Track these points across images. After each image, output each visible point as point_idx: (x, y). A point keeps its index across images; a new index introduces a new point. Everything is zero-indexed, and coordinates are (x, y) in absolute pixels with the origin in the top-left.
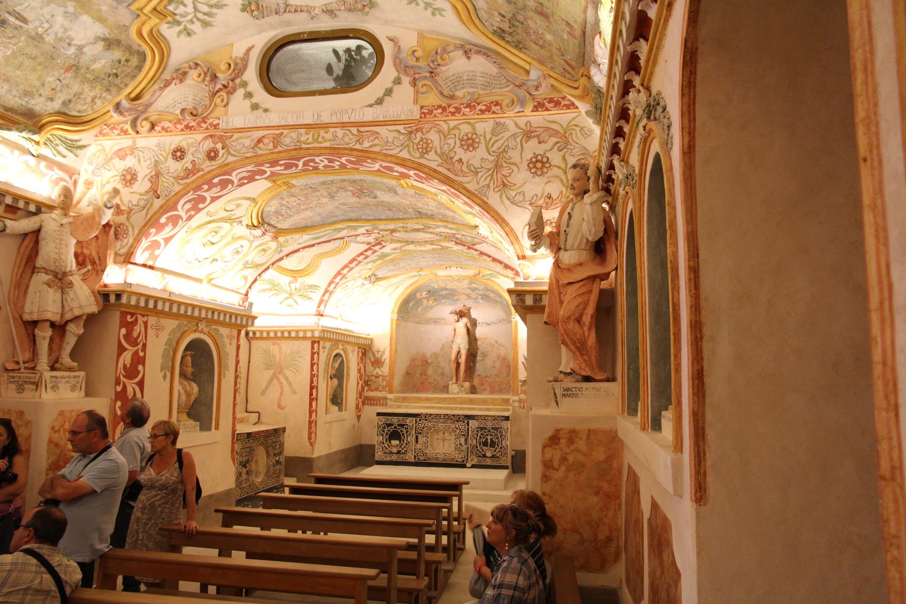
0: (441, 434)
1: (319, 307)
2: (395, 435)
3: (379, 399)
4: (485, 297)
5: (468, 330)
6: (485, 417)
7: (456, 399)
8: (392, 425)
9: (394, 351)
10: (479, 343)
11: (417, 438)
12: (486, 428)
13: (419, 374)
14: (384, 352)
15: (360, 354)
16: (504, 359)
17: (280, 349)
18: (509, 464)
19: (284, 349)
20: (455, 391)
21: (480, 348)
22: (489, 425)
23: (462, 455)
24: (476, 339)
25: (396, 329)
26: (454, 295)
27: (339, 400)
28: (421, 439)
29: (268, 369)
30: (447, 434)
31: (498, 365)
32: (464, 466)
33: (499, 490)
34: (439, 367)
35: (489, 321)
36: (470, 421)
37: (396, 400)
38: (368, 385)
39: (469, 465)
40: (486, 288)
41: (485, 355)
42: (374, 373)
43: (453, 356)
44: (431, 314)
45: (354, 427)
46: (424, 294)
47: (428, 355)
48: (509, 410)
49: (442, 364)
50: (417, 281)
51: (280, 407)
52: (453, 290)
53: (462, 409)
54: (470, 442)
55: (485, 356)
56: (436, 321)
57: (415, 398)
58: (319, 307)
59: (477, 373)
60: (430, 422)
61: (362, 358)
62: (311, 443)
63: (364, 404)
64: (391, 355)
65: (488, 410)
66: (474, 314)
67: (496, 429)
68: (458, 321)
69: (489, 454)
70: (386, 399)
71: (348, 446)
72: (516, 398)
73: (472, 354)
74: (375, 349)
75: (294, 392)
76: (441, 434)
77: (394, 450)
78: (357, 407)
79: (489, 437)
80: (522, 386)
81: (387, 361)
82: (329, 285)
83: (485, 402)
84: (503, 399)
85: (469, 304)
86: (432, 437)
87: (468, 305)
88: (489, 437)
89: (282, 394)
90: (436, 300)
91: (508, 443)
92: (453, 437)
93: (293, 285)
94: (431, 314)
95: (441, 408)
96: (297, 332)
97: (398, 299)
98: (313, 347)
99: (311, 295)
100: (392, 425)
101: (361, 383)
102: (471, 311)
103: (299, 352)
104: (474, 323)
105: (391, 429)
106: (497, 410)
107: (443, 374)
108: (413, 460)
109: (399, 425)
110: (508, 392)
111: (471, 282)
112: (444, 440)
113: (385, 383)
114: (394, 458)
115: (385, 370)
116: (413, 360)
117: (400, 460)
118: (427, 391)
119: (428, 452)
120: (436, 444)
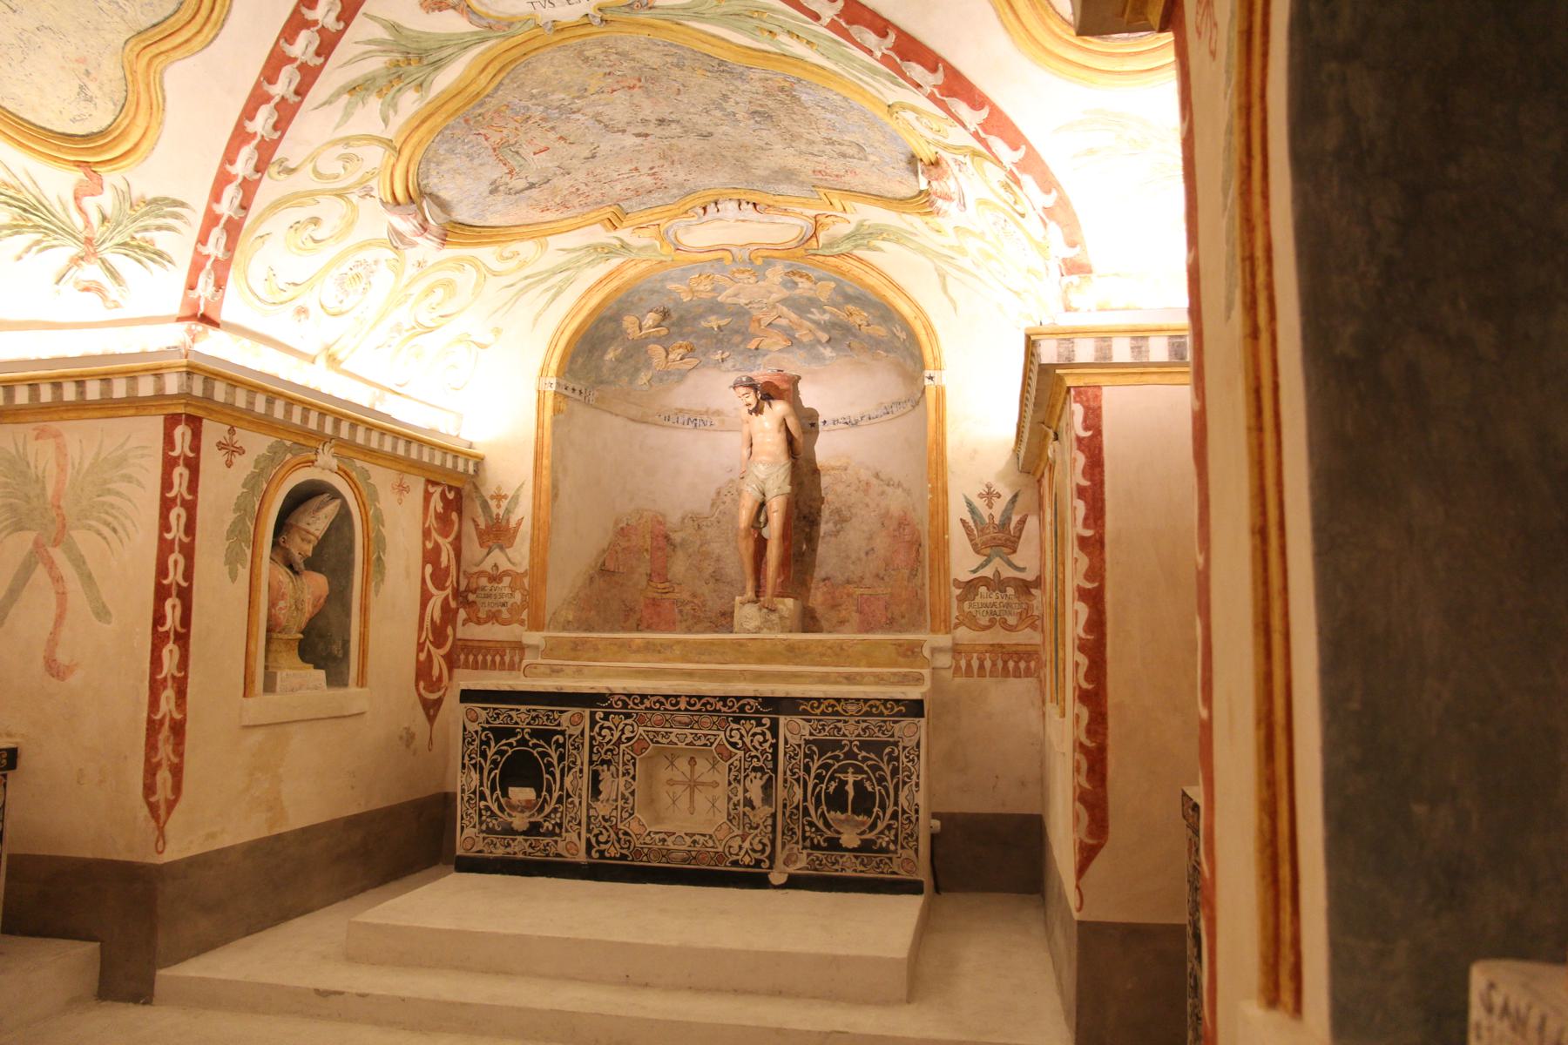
0: (683, 764)
1: (192, 287)
2: (521, 768)
3: (498, 648)
4: (841, 335)
5: (790, 441)
6: (835, 706)
7: (757, 650)
8: (510, 733)
9: (550, 492)
10: (825, 481)
11: (595, 779)
12: (837, 745)
13: (637, 576)
14: (516, 498)
15: (437, 504)
16: (903, 523)
17: (61, 450)
18: (923, 874)
19: (73, 450)
20: (752, 625)
21: (829, 497)
22: (851, 731)
23: (754, 841)
24: (816, 472)
25: (555, 423)
26: (747, 337)
27: (336, 649)
28: (611, 785)
29: (19, 527)
30: (702, 765)
31: (881, 543)
32: (758, 881)
33: (885, 1003)
34: (706, 555)
35: (854, 413)
36: (782, 720)
37: (550, 650)
38: (468, 604)
39: (777, 877)
40: (839, 290)
41: (842, 519)
42: (487, 566)
43: (744, 517)
44: (683, 396)
45: (409, 738)
46: (650, 319)
47: (674, 518)
48: (919, 680)
49: (716, 548)
50: (619, 269)
51: (54, 669)
52: (740, 313)
53: (759, 677)
54: (781, 793)
55: (844, 520)
56: (697, 420)
57: (613, 642)
58: (192, 287)
59: (819, 573)
60: (641, 721)
61: (443, 519)
62: (153, 808)
63: (451, 662)
64: (536, 507)
65: (850, 679)
66: (809, 396)
67: (875, 747)
68: (758, 410)
69: (850, 839)
70: (520, 647)
71: (378, 803)
72: (944, 640)
73: (804, 511)
74: (489, 490)
75: (102, 613)
76: (683, 764)
77: (520, 821)
78: (423, 671)
79: (851, 779)
80: (961, 599)
81: (526, 527)
82: (216, 196)
83: (839, 653)
84: (898, 645)
85: (793, 364)
86: (650, 776)
87: (791, 371)
88: (851, 779)
89: (60, 619)
90: (691, 350)
91: (921, 798)
92: (722, 776)
93: (89, 203)
94: (683, 396)
95: (690, 674)
96: (106, 379)
97: (560, 331)
98: (169, 441)
99: (162, 240)
100: (510, 733)
101: (438, 598)
102: (800, 385)
103: (121, 462)
104: (810, 422)
105: (510, 745)
106: (879, 680)
107: (717, 577)
108: (582, 858)
109: (535, 734)
110: (915, 626)
111: (790, 282)
112: (693, 785)
113: (518, 597)
114: (519, 847)
115: (519, 555)
116: (623, 532)
117: (539, 856)
118: (670, 626)
119: (634, 827)
120: (666, 800)
